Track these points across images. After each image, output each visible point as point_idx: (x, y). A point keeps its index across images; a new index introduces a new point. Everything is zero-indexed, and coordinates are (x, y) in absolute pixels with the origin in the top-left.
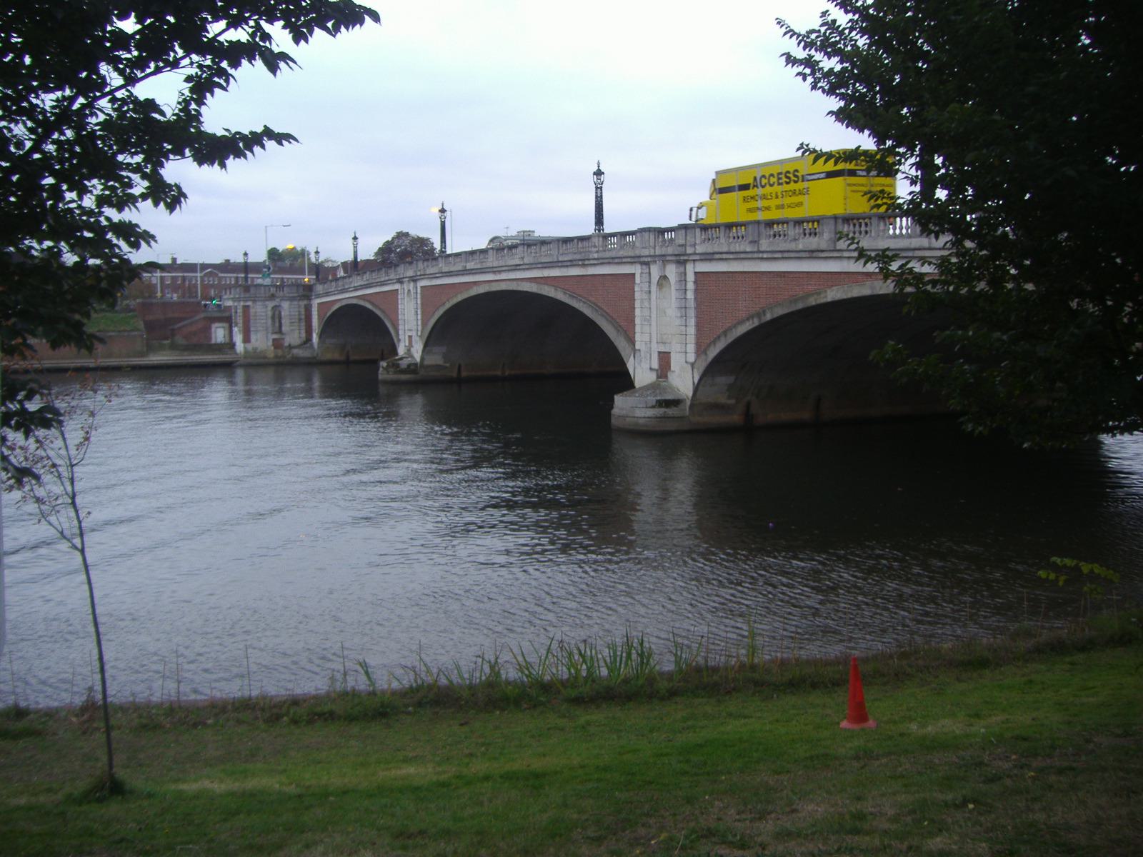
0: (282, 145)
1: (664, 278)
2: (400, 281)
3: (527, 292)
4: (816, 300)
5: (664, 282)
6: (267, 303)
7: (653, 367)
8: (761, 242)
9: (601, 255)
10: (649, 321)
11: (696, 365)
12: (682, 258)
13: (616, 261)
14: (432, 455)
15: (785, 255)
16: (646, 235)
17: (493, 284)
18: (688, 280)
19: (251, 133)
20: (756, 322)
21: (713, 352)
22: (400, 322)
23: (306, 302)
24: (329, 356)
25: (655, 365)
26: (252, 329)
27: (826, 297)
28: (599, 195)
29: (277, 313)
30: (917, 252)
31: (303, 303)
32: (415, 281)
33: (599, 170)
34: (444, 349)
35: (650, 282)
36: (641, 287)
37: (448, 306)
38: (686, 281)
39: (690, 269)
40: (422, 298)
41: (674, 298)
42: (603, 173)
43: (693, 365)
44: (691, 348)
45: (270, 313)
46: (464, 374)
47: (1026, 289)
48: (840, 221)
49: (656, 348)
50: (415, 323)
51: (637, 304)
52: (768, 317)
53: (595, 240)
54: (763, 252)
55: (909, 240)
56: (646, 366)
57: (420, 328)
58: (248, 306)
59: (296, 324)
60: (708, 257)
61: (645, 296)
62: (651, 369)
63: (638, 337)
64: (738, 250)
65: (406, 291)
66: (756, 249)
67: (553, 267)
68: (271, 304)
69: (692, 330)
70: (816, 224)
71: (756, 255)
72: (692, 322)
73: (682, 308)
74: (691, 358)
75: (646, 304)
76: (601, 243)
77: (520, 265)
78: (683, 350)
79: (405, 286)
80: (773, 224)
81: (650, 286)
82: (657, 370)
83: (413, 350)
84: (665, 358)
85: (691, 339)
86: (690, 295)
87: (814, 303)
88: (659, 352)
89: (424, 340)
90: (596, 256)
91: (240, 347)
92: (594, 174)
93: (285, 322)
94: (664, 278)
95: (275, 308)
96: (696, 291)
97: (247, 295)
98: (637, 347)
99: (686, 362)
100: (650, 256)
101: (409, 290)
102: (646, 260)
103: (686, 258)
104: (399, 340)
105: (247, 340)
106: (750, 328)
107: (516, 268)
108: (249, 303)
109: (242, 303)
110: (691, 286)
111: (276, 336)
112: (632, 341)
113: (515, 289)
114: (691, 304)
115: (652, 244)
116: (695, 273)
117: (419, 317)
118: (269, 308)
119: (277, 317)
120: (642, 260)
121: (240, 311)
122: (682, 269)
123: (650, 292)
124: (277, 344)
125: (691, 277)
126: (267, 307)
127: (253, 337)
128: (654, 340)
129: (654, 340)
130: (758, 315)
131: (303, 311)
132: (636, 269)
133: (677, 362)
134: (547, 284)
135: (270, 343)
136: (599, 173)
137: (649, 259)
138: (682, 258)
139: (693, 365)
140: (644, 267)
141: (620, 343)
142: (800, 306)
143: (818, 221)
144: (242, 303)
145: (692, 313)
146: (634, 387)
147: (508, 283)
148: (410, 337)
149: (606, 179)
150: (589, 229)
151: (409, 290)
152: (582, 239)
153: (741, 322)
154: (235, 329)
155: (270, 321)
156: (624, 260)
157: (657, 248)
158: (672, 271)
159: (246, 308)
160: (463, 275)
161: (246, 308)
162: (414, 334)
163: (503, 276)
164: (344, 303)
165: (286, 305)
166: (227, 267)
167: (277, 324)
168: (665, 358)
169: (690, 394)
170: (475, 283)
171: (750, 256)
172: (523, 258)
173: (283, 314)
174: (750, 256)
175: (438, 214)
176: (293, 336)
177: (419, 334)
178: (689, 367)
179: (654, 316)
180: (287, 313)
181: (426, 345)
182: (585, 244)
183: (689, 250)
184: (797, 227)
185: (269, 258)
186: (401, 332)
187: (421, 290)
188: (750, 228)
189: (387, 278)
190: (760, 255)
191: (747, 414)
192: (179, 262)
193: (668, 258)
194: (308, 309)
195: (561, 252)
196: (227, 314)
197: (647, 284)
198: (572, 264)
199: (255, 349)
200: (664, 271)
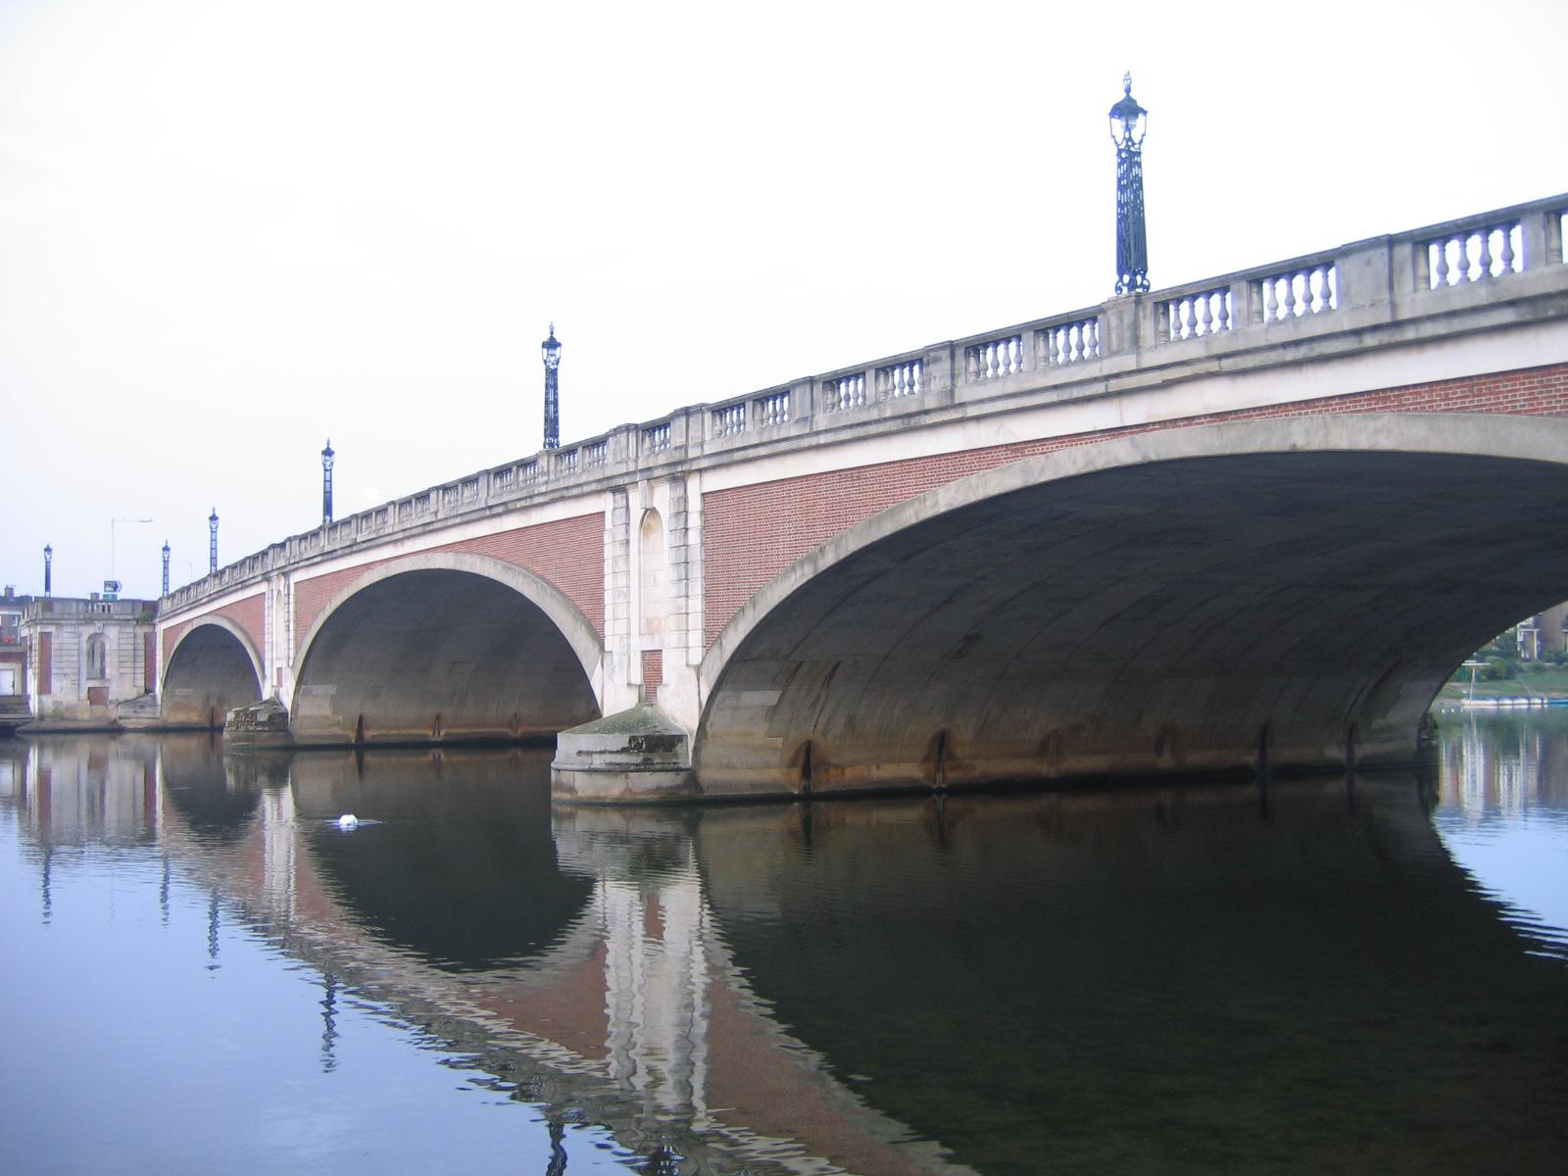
1: (651, 512)
2: (266, 578)
3: (440, 569)
4: (916, 514)
5: (652, 522)
6: (81, 628)
7: (633, 681)
8: (816, 419)
9: (551, 487)
10: (627, 595)
11: (703, 670)
12: (679, 469)
13: (575, 492)
14: (1501, 822)
16: (622, 438)
18: (690, 510)
21: (734, 639)
22: (267, 647)
23: (146, 629)
24: (180, 717)
25: (637, 677)
26: (54, 671)
27: (936, 503)
28: (551, 391)
29: (98, 645)
30: (1113, 382)
31: (141, 631)
32: (286, 575)
33: (552, 338)
34: (331, 689)
35: (628, 524)
36: (614, 536)
37: (329, 610)
38: (686, 512)
39: (695, 487)
40: (296, 603)
41: (666, 546)
42: (559, 345)
43: (698, 669)
44: (696, 638)
45: (85, 647)
46: (368, 734)
48: (960, 353)
49: (639, 644)
50: (286, 646)
51: (608, 569)
53: (543, 463)
54: (818, 433)
55: (1098, 365)
56: (620, 679)
57: (292, 655)
58: (50, 634)
59: (130, 664)
60: (725, 460)
61: (620, 551)
62: (629, 685)
63: (608, 629)
64: (775, 437)
65: (275, 593)
66: (807, 431)
68: (87, 631)
69: (697, 604)
70: (916, 368)
71: (806, 442)
72: (697, 588)
73: (678, 564)
74: (696, 656)
75: (622, 565)
76: (552, 468)
77: (432, 523)
78: (683, 644)
79: (274, 585)
80: (839, 381)
81: (627, 531)
82: (640, 686)
83: (282, 691)
84: (652, 661)
85: (696, 621)
86: (694, 538)
87: (914, 521)
88: (644, 652)
89: (297, 675)
90: (543, 489)
91: (34, 705)
92: (545, 345)
93: (111, 662)
94: (651, 512)
95: (93, 637)
96: (704, 528)
97: (48, 615)
98: (607, 648)
99: (687, 665)
100: (627, 474)
101: (279, 592)
102: (621, 481)
103: (686, 468)
104: (264, 676)
105: (44, 688)
106: (798, 585)
107: (427, 529)
108: (51, 629)
109: (39, 629)
110: (695, 521)
111: (92, 684)
112: (598, 638)
113: (423, 567)
114: (696, 554)
115: (632, 453)
117: (292, 634)
118: (85, 638)
119: (95, 652)
120: (614, 483)
121: (36, 642)
122: (680, 492)
123: (628, 542)
124: (96, 696)
125: (695, 504)
126: (80, 636)
127: (56, 684)
128: (635, 631)
129: (635, 631)
130: (812, 559)
131: (141, 641)
132: (605, 503)
133: (672, 666)
134: (471, 553)
135: (84, 694)
137: (627, 480)
138: (679, 469)
139: (698, 669)
140: (618, 496)
143: (920, 361)
144: (39, 629)
145: (697, 572)
146: (601, 716)
147: (413, 558)
148: (279, 670)
150: (532, 443)
151: (279, 592)
152: (524, 464)
154: (30, 672)
155: (84, 659)
157: (640, 460)
158: (663, 496)
159: (45, 638)
160: (351, 553)
161: (45, 638)
162: (283, 664)
164: (196, 624)
165: (112, 633)
167: (98, 665)
168: (652, 661)
169: (695, 725)
170: (368, 566)
171: (794, 445)
172: (436, 513)
173: (107, 647)
174: (794, 445)
176: (123, 686)
177: (291, 663)
178: (693, 674)
179: (634, 584)
180: (115, 647)
181: (300, 682)
182: (530, 471)
183: (693, 453)
184: (882, 379)
186: (267, 664)
187: (296, 590)
188: (797, 393)
189: (251, 576)
190: (814, 441)
191: (807, 758)
192: (17, 593)
193: (657, 473)
194: (149, 640)
195: (492, 493)
196: (19, 650)
197: (623, 529)
198: (508, 510)
199: (57, 703)
200: (652, 498)
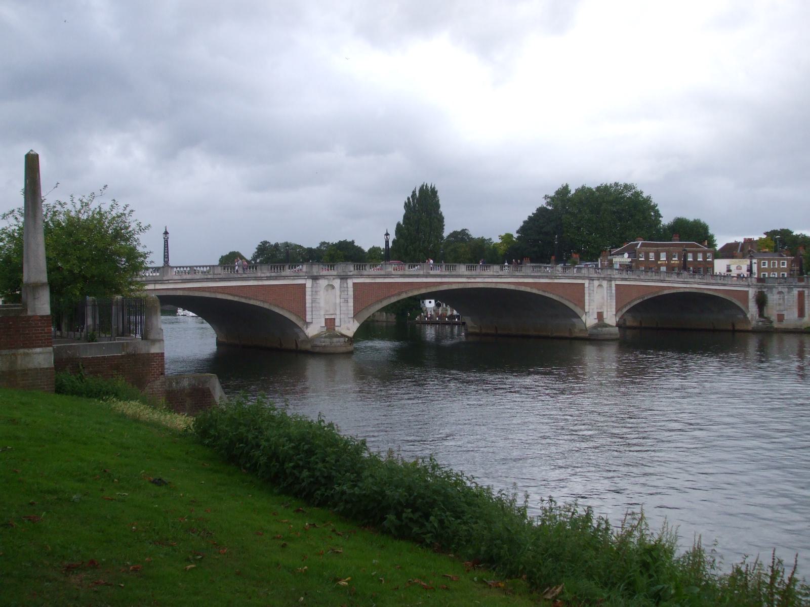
0: (765, 234)
15: (649, 281)
17: (498, 284)
19: (781, 229)
20: (641, 300)
46: (643, 325)
47: (21, 317)
52: (646, 298)
67: (203, 281)
116: (616, 285)
125: (613, 286)
132: (586, 282)
136: (166, 233)
141: (577, 310)
142: (656, 295)
149: (170, 236)
153: (635, 299)
156: (170, 281)
163: (473, 280)
166: (298, 245)
175: (162, 237)
185: (275, 245)
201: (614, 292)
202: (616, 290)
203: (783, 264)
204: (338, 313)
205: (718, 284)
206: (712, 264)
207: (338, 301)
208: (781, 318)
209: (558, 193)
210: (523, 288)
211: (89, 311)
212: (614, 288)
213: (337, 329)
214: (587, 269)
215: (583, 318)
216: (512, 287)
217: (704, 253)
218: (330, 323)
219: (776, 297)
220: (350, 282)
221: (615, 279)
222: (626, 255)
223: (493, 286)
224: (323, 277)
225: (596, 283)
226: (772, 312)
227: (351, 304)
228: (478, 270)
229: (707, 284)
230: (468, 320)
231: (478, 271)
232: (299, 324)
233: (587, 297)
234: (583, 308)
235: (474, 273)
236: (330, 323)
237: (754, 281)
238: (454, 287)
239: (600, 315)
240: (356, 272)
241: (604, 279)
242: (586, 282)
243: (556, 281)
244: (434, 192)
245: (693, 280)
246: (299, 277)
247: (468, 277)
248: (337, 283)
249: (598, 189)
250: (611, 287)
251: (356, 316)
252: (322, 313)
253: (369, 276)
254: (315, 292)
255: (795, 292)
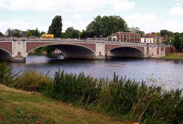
132: (96, 44)
141: (93, 51)
158: (102, 44)
201: (104, 46)
202: (105, 46)
203: (160, 40)
204: (22, 50)
205: (135, 45)
206: (140, 39)
207: (22, 47)
208: (153, 54)
209: (97, 17)
210: (77, 45)
211: (15, 103)
212: (26, 44)
213: (21, 55)
214: (96, 40)
215: (95, 54)
216: (74, 44)
217: (138, 36)
218: (19, 53)
219: (152, 49)
220: (25, 42)
221: (105, 43)
222: (116, 36)
223: (68, 44)
224: (17, 40)
225: (99, 44)
226: (150, 53)
227: (26, 47)
228: (64, 39)
229: (132, 45)
230: (64, 53)
231: (64, 40)
232: (10, 53)
233: (96, 48)
234: (95, 51)
235: (63, 40)
236: (19, 53)
237: (146, 44)
238: (57, 44)
239: (100, 53)
240: (27, 39)
241: (101, 43)
242: (96, 44)
243: (87, 43)
244: (60, 17)
245: (128, 44)
246: (10, 40)
247: (81, 42)
248: (21, 42)
249: (62, 23)
250: (103, 45)
251: (27, 51)
252: (17, 50)
253: (31, 40)
254: (15, 45)
255: (156, 47)
